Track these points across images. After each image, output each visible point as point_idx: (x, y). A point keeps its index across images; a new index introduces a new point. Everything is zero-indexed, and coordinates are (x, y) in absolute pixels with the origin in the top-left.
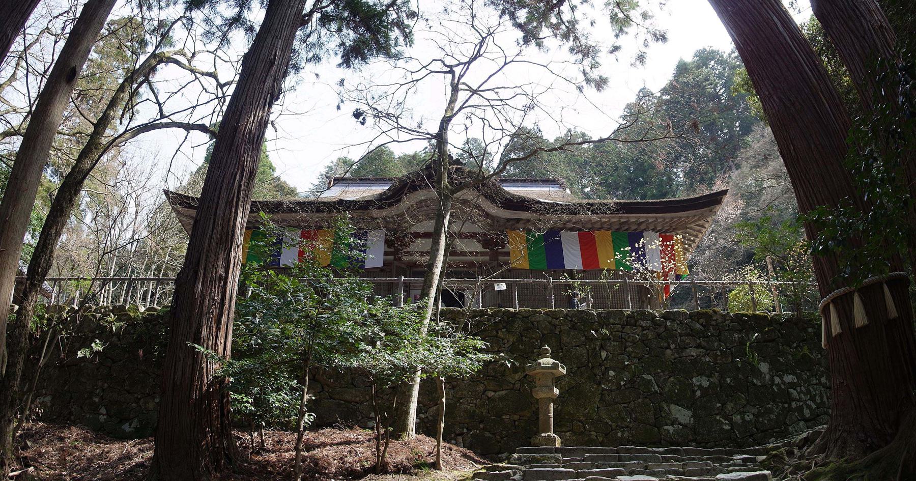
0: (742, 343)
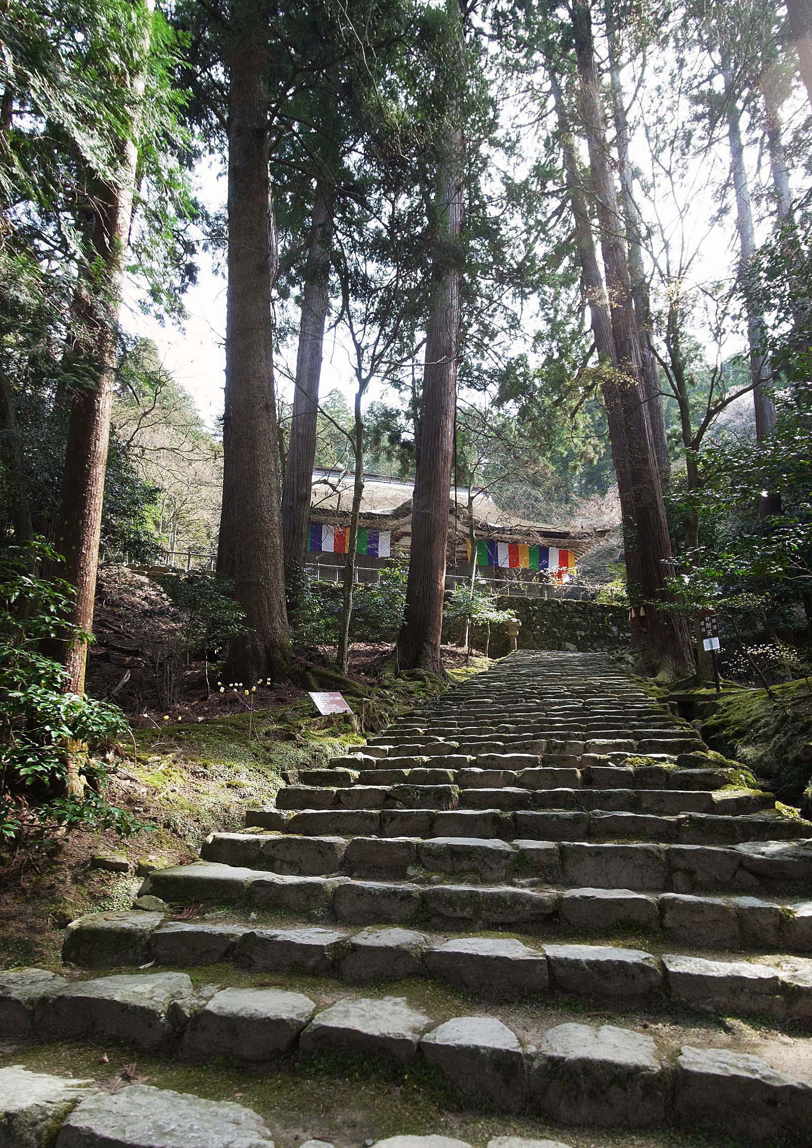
0: (603, 617)
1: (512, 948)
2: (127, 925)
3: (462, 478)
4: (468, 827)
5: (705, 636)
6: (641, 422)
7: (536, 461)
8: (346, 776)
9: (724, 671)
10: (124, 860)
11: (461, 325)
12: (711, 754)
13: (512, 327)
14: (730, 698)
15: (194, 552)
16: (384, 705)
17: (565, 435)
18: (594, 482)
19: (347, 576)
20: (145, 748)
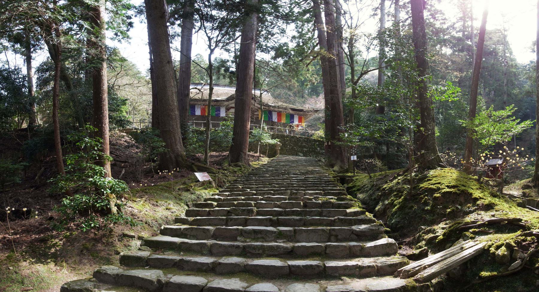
1: (276, 262)
2: (139, 255)
3: (257, 85)
4: (260, 223)
5: (352, 155)
6: (335, 72)
7: (290, 81)
8: (212, 204)
9: (358, 167)
10: (133, 234)
11: (258, 30)
12: (349, 197)
13: (281, 33)
14: (357, 177)
15: (142, 121)
16: (225, 177)
17: (303, 72)
18: (314, 92)
19: (207, 125)
20: (134, 196)
